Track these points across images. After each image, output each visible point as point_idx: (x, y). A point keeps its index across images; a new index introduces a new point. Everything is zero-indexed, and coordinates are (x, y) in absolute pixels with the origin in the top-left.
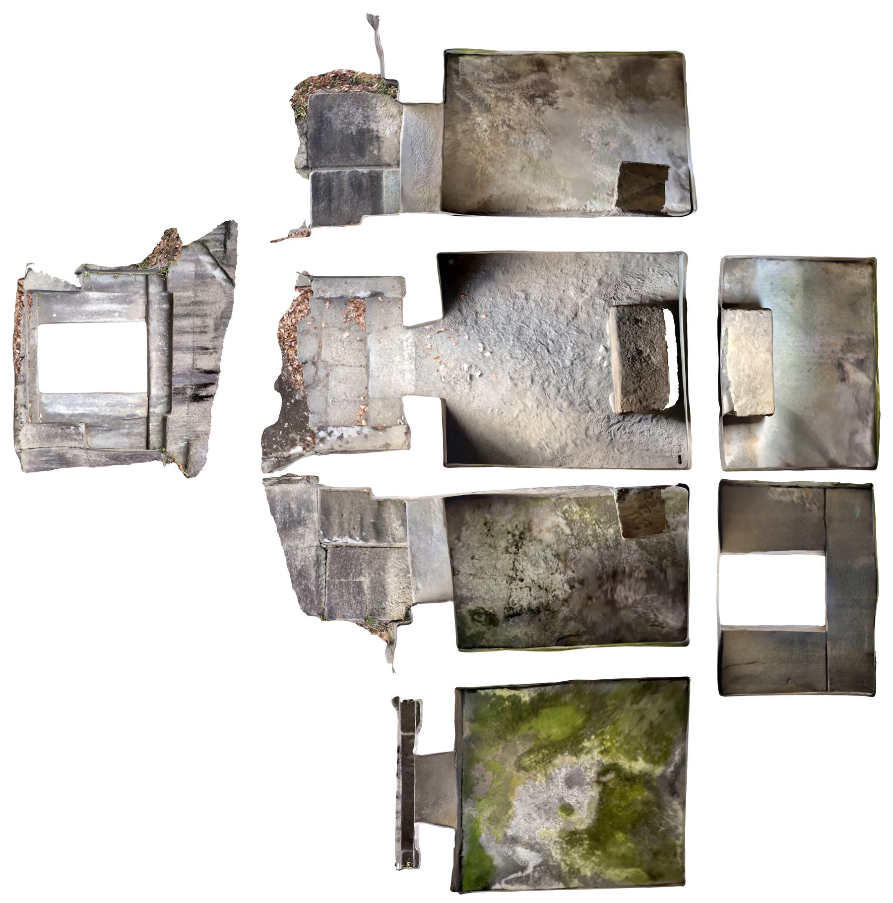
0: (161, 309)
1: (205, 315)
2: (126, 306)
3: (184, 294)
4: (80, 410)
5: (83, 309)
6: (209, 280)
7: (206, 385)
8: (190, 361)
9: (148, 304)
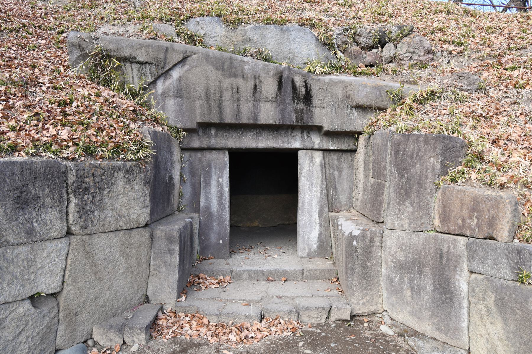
0: (216, 136)
1: (220, 88)
3: (198, 110)
4: (316, 216)
6: (183, 83)
7: (294, 88)
9: (210, 149)
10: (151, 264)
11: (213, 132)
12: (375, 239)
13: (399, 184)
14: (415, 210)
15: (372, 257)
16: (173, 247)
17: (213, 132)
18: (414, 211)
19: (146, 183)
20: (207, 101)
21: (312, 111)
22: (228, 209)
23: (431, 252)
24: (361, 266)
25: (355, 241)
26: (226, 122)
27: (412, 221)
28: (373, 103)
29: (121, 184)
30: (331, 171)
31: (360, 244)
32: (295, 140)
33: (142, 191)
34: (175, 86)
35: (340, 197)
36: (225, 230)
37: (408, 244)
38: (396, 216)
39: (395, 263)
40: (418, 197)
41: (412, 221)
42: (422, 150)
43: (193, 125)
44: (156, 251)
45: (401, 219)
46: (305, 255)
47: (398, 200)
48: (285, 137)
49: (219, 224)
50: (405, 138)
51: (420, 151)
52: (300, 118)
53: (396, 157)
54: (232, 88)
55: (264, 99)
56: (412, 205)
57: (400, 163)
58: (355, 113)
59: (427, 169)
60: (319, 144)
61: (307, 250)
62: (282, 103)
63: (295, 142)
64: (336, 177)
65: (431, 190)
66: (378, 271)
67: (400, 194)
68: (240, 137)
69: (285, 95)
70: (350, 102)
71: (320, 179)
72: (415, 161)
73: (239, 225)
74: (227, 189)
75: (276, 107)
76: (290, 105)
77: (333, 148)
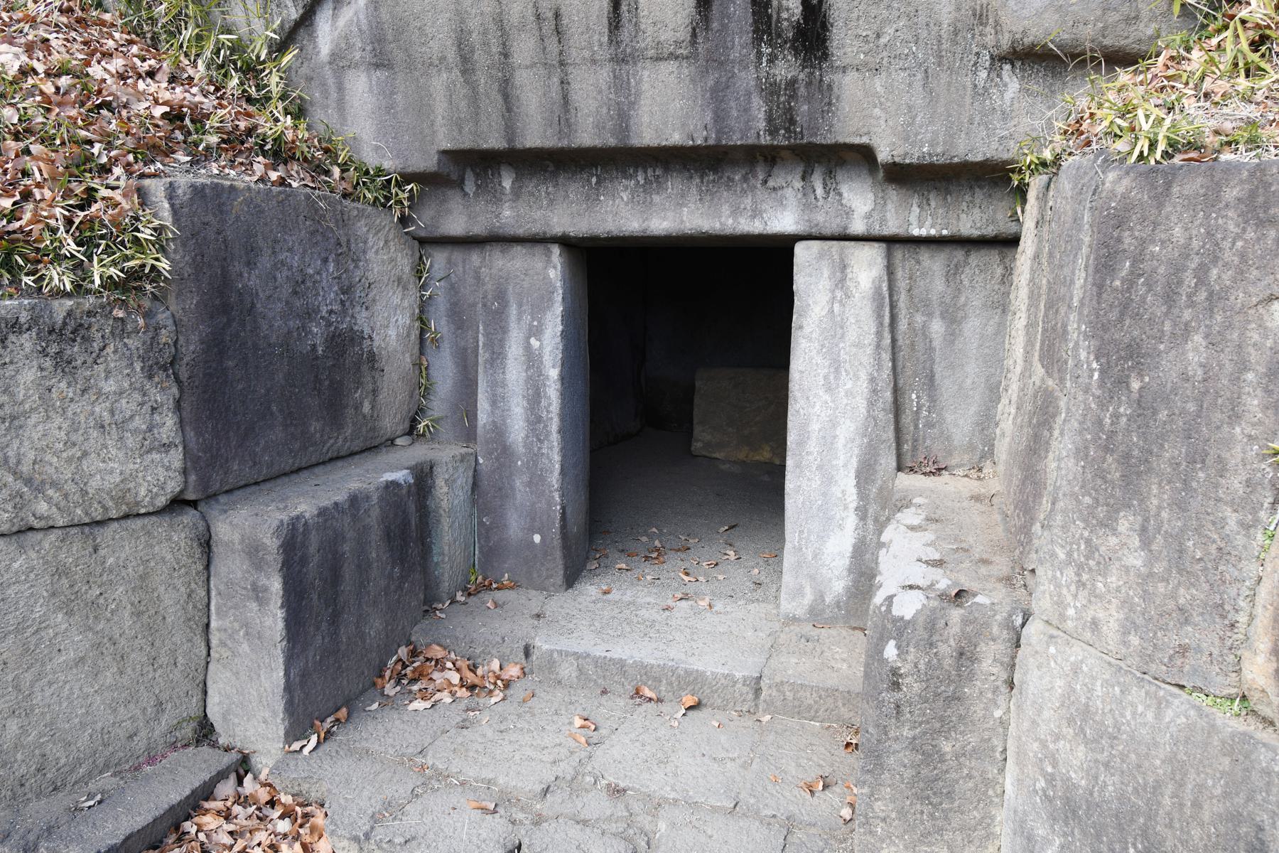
0: (517, 194)
2: (513, 310)
3: (440, 108)
4: (847, 484)
5: (521, 450)
8: (668, 69)
10: (213, 624)
11: (507, 183)
12: (982, 647)
13: (1100, 422)
14: (1159, 568)
15: (961, 717)
16: (263, 581)
17: (507, 183)
18: (1151, 575)
19: (161, 364)
20: (464, 72)
21: (830, 87)
22: (555, 437)
23: (1206, 816)
24: (913, 745)
25: (892, 643)
26: (529, 144)
27: (1140, 621)
28: (1087, 34)
29: (29, 375)
30: (919, 319)
31: (910, 658)
32: (781, 203)
33: (137, 396)
34: (364, 28)
35: (949, 417)
36: (550, 503)
37: (1109, 722)
38: (1070, 572)
39: (1050, 779)
40: (1180, 506)
41: (1140, 621)
42: (1227, 256)
43: (425, 162)
44: (222, 587)
45: (1093, 593)
46: (800, 612)
47: (1088, 500)
48: (744, 191)
49: (530, 484)
50: (1153, 186)
51: (1215, 260)
52: (783, 119)
53: (1100, 287)
54: (538, 17)
55: (651, 53)
56: (1146, 543)
57: (1113, 316)
58: (1011, 82)
59: (1243, 366)
60: (868, 216)
61: (808, 598)
62: (716, 61)
63: (778, 214)
64: (937, 344)
65: (1248, 483)
66: (989, 783)
67: (1101, 474)
68: (592, 199)
69: (724, 27)
70: (990, 40)
71: (869, 350)
72: (1187, 315)
73: (716, 455)
74: (554, 373)
75: (693, 81)
76: (746, 68)
77: (923, 232)
